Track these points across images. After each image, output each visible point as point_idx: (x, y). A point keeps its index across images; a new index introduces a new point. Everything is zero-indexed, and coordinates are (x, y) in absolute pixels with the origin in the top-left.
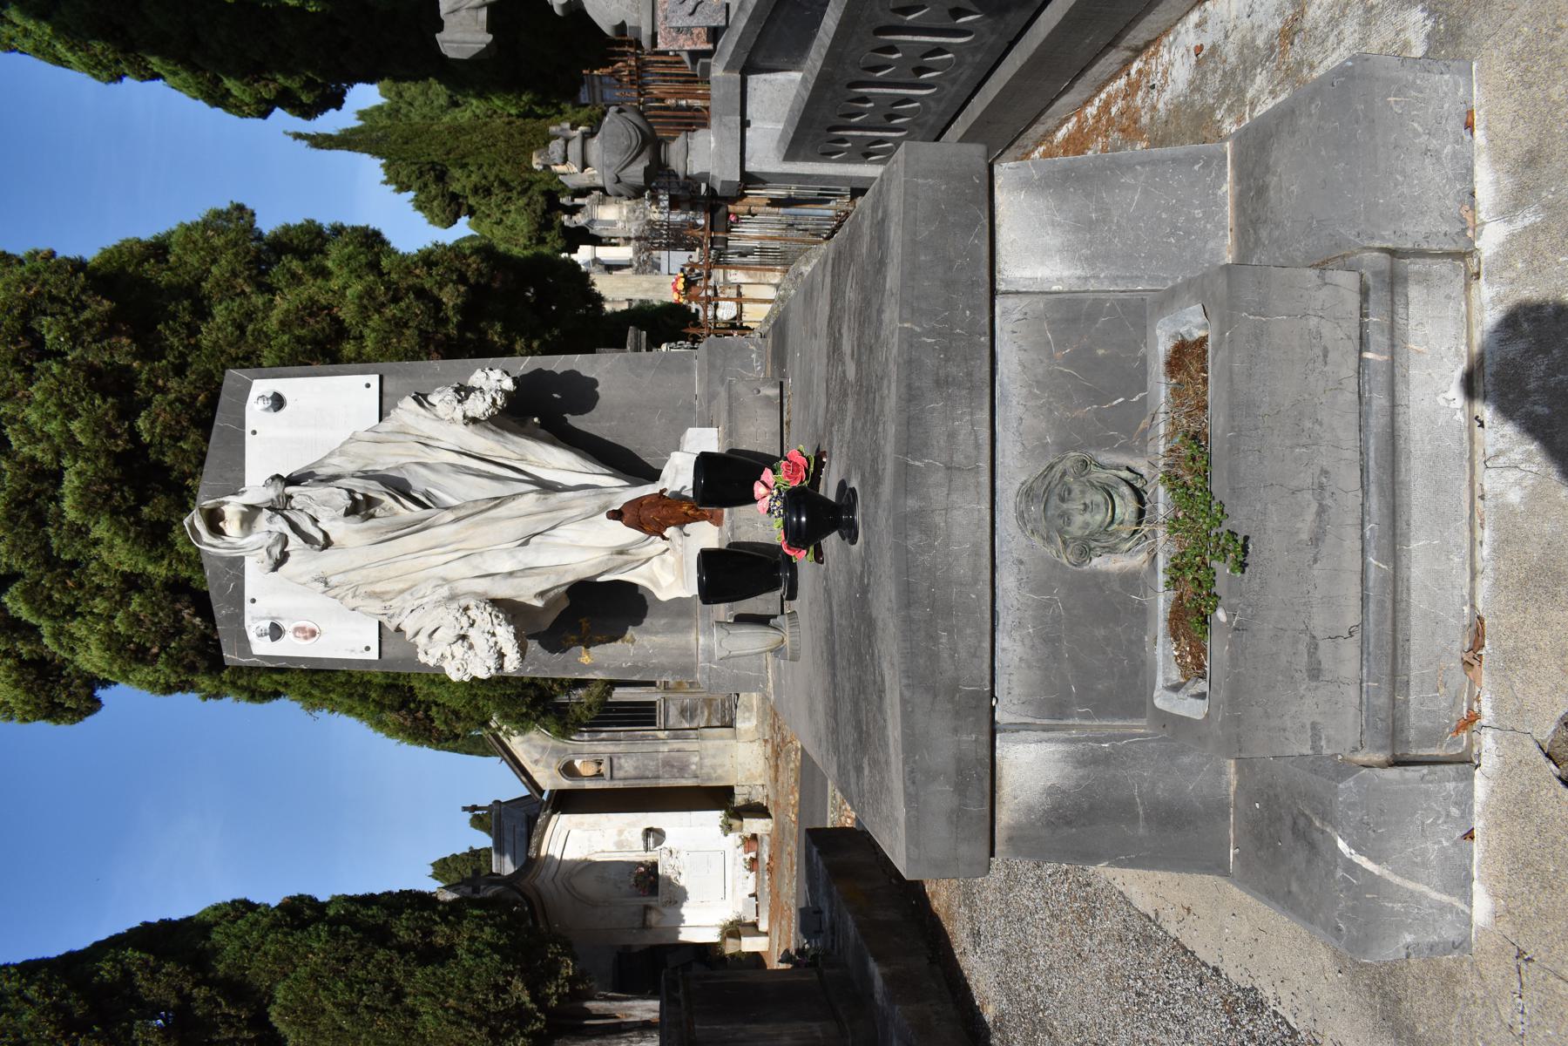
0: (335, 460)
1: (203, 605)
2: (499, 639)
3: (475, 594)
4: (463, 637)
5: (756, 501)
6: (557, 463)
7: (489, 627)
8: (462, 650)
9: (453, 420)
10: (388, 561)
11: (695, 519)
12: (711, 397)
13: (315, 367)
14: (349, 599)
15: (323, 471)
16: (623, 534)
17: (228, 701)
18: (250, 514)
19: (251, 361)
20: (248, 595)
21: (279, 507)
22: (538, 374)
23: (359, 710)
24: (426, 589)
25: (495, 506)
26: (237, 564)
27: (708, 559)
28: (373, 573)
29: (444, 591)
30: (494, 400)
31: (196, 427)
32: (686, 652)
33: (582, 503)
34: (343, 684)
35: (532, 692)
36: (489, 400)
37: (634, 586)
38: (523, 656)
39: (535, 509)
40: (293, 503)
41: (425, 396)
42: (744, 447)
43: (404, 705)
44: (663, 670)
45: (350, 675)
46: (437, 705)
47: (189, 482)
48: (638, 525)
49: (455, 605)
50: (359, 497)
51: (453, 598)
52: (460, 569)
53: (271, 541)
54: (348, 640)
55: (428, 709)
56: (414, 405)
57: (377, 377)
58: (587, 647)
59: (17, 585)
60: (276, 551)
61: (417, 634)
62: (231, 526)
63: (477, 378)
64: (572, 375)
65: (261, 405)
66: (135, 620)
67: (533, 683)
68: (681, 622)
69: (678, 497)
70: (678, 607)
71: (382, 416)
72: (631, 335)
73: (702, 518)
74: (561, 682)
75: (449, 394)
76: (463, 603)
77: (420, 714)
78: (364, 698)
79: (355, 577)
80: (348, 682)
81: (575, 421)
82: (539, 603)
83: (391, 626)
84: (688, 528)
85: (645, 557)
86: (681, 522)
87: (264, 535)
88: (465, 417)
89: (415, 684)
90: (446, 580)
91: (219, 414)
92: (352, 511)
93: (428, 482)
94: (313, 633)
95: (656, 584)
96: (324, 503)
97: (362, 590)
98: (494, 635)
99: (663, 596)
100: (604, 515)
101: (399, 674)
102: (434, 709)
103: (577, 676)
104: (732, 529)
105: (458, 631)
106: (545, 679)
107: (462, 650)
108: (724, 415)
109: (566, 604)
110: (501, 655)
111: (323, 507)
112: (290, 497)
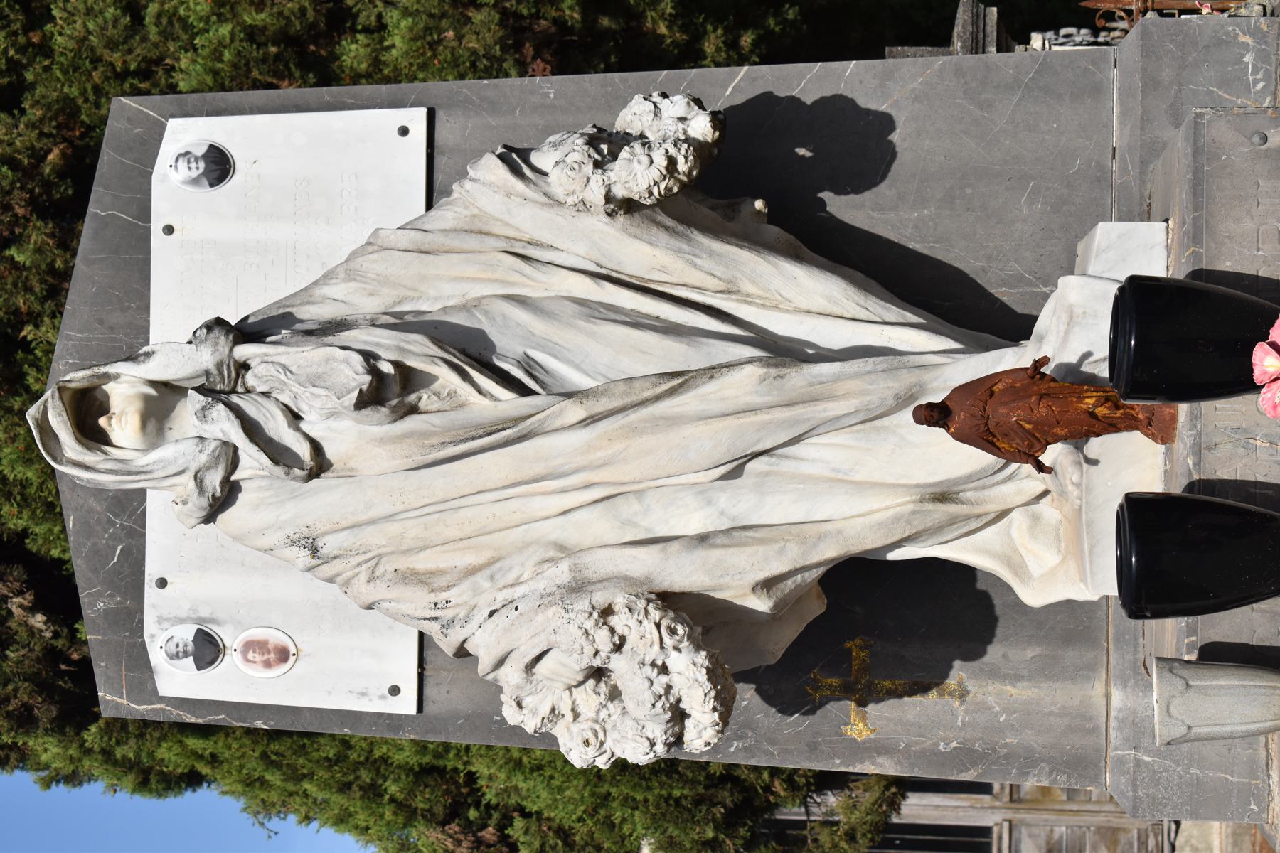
0: (336, 290)
1: (56, 591)
2: (675, 680)
3: (626, 581)
4: (598, 674)
5: (1256, 388)
6: (804, 299)
7: (654, 653)
8: (595, 701)
9: (583, 206)
10: (446, 505)
11: (1112, 427)
12: (1150, 151)
13: (289, 92)
14: (360, 586)
15: (312, 313)
16: (949, 456)
17: (94, 791)
18: (161, 402)
19: (150, 77)
20: (152, 570)
21: (221, 388)
22: (766, 101)
23: (361, 818)
24: (522, 566)
25: (672, 392)
26: (130, 506)
27: (1140, 515)
28: (411, 530)
29: (561, 573)
30: (672, 162)
31: (43, 217)
32: (1083, 722)
33: (860, 387)
34: (330, 763)
35: (727, 796)
36: (661, 162)
37: (966, 573)
38: (725, 718)
39: (758, 400)
40: (250, 379)
41: (524, 154)
42: (1227, 265)
43: (455, 812)
44: (1029, 761)
45: (346, 743)
46: (525, 815)
47: (28, 332)
48: (983, 438)
49: (584, 604)
50: (387, 368)
51: (578, 587)
52: (595, 527)
53: (203, 458)
54: (357, 673)
55: (506, 822)
56: (502, 171)
57: (422, 112)
58: (862, 703)
59: (1036, 690)
60: (214, 480)
61: (500, 663)
62: (123, 425)
63: (634, 115)
64: (838, 107)
65: (185, 172)
67: (730, 776)
68: (1072, 656)
69: (1074, 378)
70: (1069, 622)
71: (429, 205)
72: (963, 16)
73: (1129, 423)
74: (790, 778)
75: (577, 149)
76: (601, 599)
77: (489, 834)
78: (373, 793)
79: (374, 538)
80: (340, 759)
81: (842, 207)
82: (761, 604)
83: (447, 645)
84: (1095, 446)
85: (994, 508)
86: (1080, 432)
87: (190, 447)
88: (609, 198)
89: (481, 767)
90: (564, 550)
91: (97, 192)
92: (370, 398)
93: (530, 338)
94: (283, 655)
95: (1019, 568)
96: (314, 381)
97: (387, 566)
98: (664, 670)
99: (1033, 597)
100: (907, 415)
101: (447, 747)
102: (519, 823)
103: (838, 765)
104: (1198, 451)
105: (587, 661)
106: (757, 769)
107: (595, 701)
108: (1182, 194)
109: (817, 607)
110: (679, 716)
111: (311, 386)
112: (244, 367)
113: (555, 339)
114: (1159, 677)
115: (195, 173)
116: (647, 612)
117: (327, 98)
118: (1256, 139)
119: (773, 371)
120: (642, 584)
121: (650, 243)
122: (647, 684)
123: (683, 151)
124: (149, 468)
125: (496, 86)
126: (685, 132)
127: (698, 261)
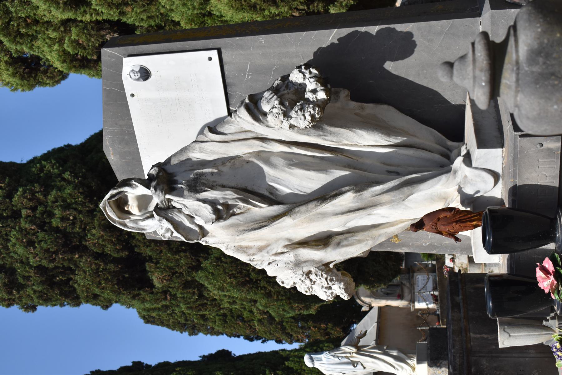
3: (313, 262)
57: (215, 52)
66: (76, 44)
76: (306, 270)
113: (278, 176)
114: (500, 333)
115: (137, 77)
116: (322, 275)
117: (179, 46)
118: (538, 146)
119: (358, 194)
120: (320, 262)
121: (308, 135)
122: (324, 293)
123: (316, 111)
124: (144, 228)
125: (241, 40)
126: (316, 97)
127: (326, 138)
